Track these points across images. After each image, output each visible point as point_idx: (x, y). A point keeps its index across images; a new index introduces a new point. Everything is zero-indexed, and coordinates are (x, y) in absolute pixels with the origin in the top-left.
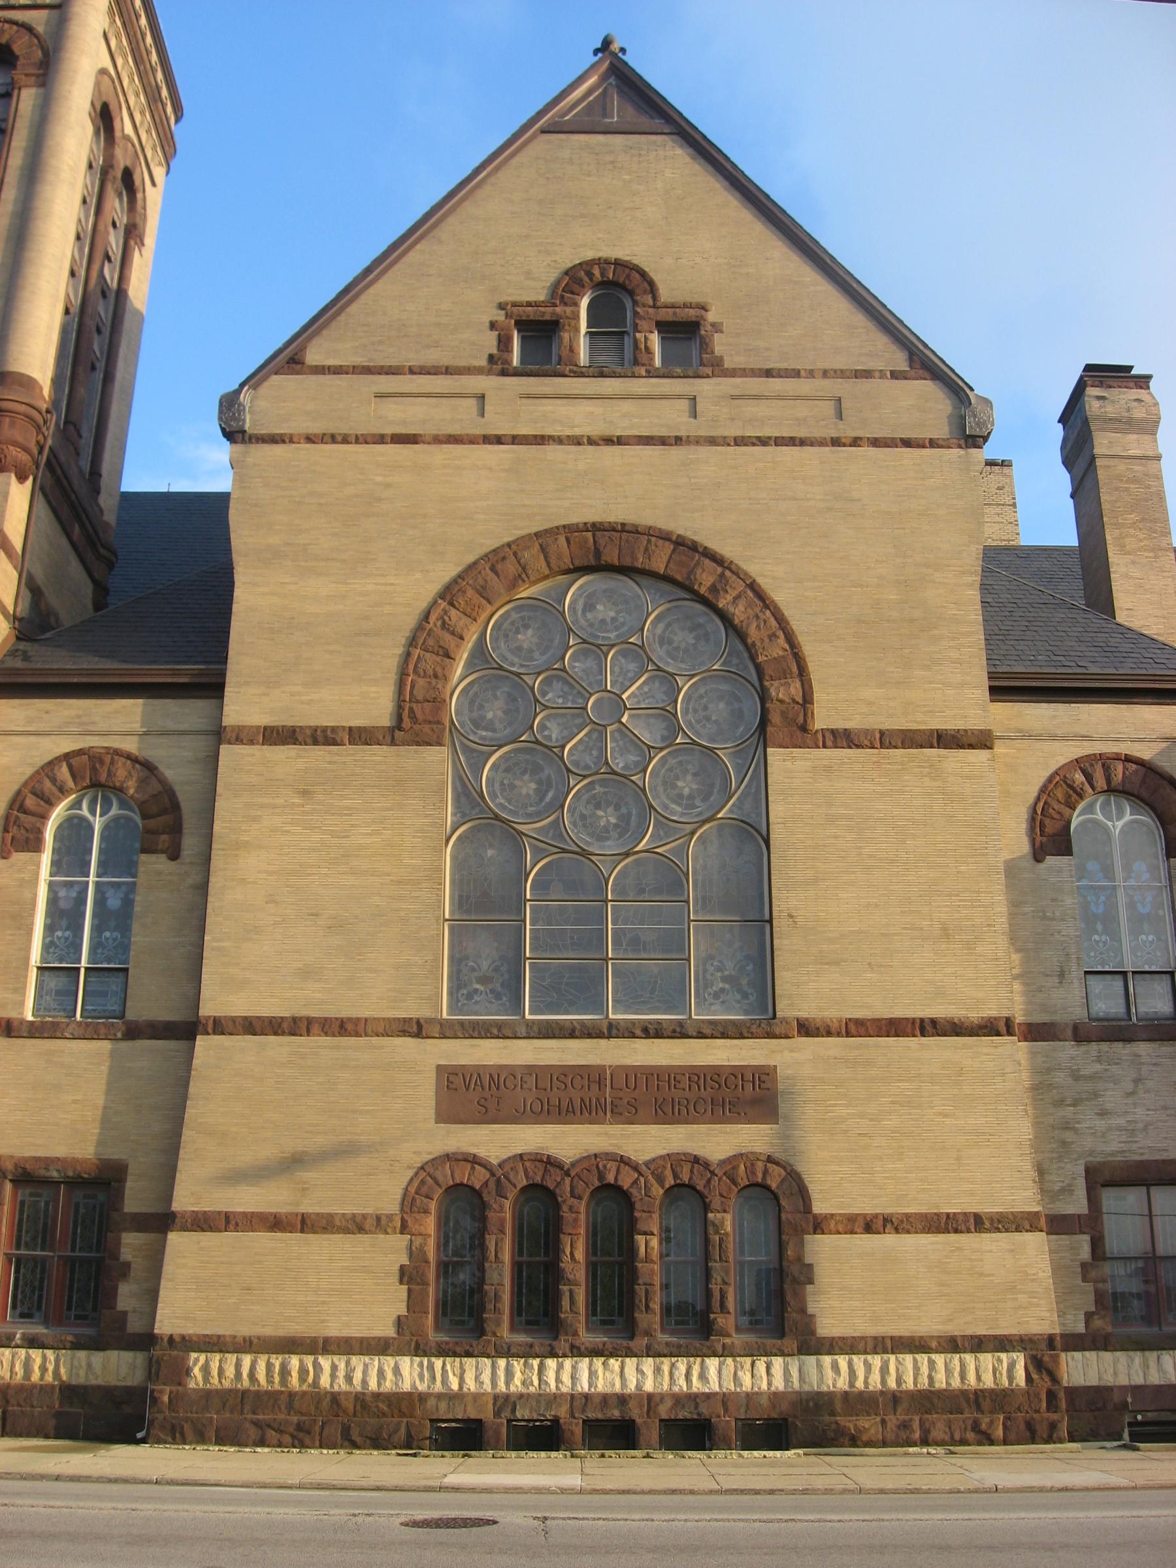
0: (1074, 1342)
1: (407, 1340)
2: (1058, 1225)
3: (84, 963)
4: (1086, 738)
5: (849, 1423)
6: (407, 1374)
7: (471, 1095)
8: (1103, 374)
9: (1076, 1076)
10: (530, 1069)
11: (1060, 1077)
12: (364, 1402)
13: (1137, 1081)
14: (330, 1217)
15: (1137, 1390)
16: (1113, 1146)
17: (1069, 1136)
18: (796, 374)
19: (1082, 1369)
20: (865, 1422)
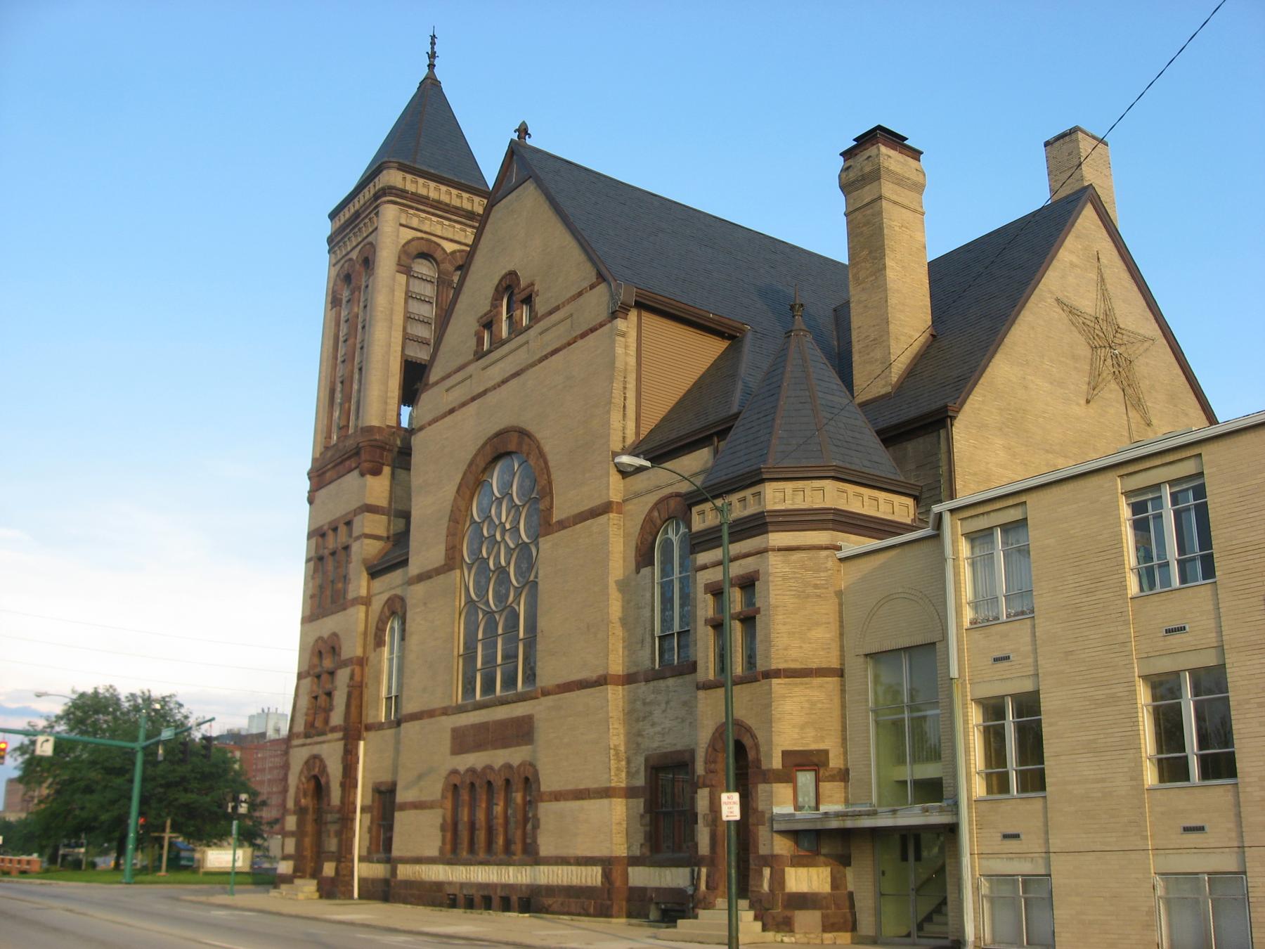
0: (634, 861)
1: (442, 860)
2: (630, 793)
3: (1003, 588)
4: (659, 488)
5: (549, 901)
6: (438, 873)
7: (463, 741)
8: (878, 136)
9: (644, 704)
10: (473, 726)
11: (639, 705)
12: (439, 886)
13: (667, 703)
14: (588, 790)
15: (657, 890)
16: (656, 745)
17: (640, 740)
18: (557, 308)
19: (641, 877)
20: (550, 901)
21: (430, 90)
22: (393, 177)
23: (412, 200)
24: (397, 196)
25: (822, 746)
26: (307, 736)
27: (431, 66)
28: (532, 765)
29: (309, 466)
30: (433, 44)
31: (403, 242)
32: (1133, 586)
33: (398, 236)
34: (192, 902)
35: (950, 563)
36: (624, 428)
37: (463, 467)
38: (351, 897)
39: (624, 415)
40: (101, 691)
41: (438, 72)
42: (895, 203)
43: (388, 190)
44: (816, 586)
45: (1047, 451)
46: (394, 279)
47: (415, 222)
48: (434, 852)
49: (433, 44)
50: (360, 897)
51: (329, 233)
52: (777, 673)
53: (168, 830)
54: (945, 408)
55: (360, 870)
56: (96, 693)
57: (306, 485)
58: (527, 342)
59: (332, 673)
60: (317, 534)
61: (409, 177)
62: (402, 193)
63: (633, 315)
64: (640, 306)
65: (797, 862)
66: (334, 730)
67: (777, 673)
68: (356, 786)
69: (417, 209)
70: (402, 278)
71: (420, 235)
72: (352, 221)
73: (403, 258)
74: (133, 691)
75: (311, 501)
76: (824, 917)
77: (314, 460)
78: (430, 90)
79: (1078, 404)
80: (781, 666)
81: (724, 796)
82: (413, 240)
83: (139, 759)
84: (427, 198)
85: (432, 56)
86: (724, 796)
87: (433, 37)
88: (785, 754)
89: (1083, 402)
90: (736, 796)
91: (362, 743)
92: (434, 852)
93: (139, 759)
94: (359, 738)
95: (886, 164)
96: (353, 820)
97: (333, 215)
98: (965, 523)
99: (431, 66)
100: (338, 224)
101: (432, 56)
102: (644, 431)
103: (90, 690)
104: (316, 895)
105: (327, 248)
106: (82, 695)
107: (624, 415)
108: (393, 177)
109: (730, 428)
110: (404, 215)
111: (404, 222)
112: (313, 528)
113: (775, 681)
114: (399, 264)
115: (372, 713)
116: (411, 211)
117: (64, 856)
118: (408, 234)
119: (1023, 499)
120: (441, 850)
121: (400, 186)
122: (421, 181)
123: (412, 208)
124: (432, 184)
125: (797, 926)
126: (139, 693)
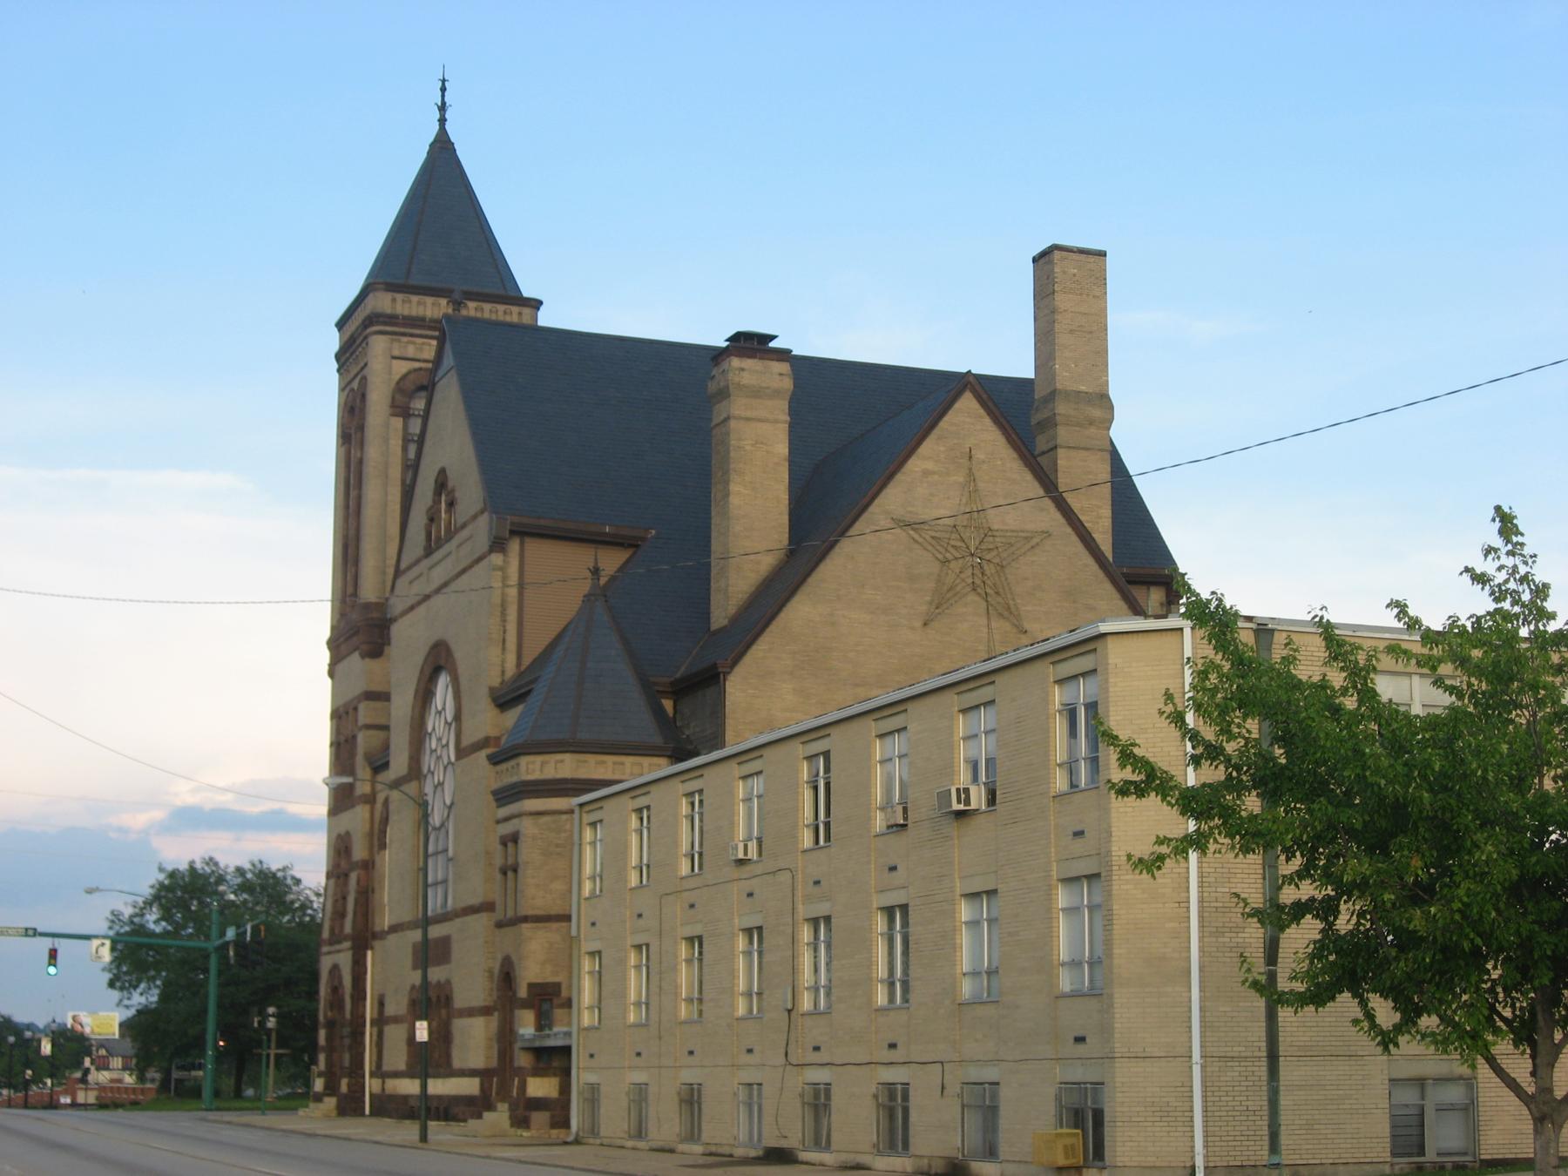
21: (442, 152)
22: (383, 302)
23: (404, 325)
24: (385, 324)
25: (556, 979)
26: (331, 944)
27: (442, 121)
28: (448, 982)
29: (327, 633)
30: (443, 89)
31: (397, 377)
32: (807, 840)
33: (390, 373)
34: (238, 1125)
35: (576, 848)
36: (503, 661)
37: (417, 674)
38: (363, 1114)
39: (504, 649)
40: (198, 865)
41: (450, 127)
42: (748, 419)
43: (373, 319)
44: (557, 846)
45: (857, 685)
46: (387, 425)
47: (411, 351)
48: (402, 1066)
49: (443, 89)
50: (373, 1114)
51: (336, 347)
52: (526, 919)
53: (273, 1045)
54: (715, 666)
55: (371, 1085)
56: (192, 869)
57: (325, 656)
58: (471, 537)
59: (346, 875)
60: (342, 715)
61: (399, 297)
62: (391, 319)
63: (514, 546)
64: (513, 533)
65: (538, 1072)
66: (346, 938)
67: (526, 919)
68: (365, 999)
69: (412, 335)
70: (398, 423)
71: (417, 365)
72: (357, 330)
73: (398, 397)
74: (239, 863)
75: (331, 674)
76: (552, 1117)
77: (333, 628)
78: (442, 152)
79: (913, 628)
80: (530, 912)
81: (418, 1024)
82: (409, 373)
83: (213, 962)
84: (423, 319)
85: (443, 108)
86: (418, 1024)
87: (444, 81)
88: (531, 986)
89: (918, 624)
90: (425, 1024)
91: (369, 953)
92: (402, 1066)
93: (213, 962)
94: (366, 948)
95: (737, 379)
96: (363, 1034)
97: (341, 325)
98: (880, 723)
99: (442, 121)
100: (348, 334)
101: (443, 108)
102: (527, 661)
103: (183, 866)
104: (334, 1113)
105: (336, 366)
106: (173, 875)
107: (504, 649)
108: (383, 302)
109: (530, 691)
110: (396, 345)
111: (396, 353)
112: (341, 702)
113: (524, 925)
114: (393, 405)
115: (377, 921)
116: (405, 339)
117: (179, 1081)
118: (401, 368)
119: (827, 731)
120: (408, 1064)
121: (389, 311)
122: (415, 298)
123: (404, 334)
124: (429, 300)
125: (533, 1124)
126: (247, 866)
